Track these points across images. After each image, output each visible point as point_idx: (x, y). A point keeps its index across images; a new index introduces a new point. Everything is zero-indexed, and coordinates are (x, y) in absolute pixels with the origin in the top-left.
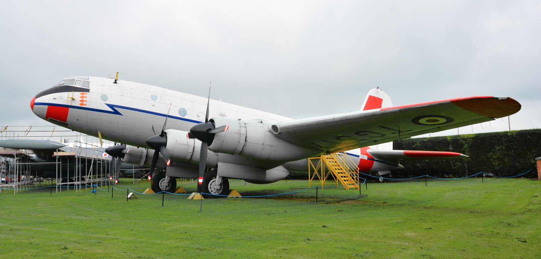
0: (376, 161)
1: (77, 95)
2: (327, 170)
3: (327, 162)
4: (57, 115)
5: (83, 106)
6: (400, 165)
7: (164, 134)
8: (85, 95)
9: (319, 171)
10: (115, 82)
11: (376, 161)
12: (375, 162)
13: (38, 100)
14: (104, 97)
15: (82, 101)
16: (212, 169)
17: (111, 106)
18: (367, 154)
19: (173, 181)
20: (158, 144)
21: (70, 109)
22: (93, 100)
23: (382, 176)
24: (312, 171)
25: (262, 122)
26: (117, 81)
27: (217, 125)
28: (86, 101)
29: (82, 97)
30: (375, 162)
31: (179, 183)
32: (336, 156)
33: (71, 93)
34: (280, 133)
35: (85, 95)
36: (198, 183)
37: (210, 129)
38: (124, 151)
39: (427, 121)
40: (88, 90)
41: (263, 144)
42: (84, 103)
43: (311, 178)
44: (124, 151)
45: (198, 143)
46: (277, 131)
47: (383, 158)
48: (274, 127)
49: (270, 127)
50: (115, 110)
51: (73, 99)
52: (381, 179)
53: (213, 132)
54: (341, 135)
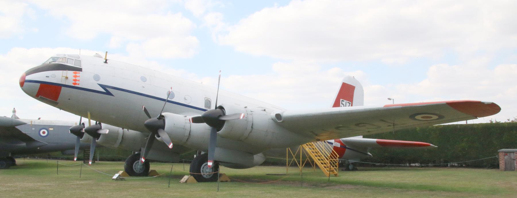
0: (348, 148)
1: (70, 74)
2: (304, 157)
3: (307, 149)
4: (48, 93)
5: (77, 86)
6: (369, 154)
7: (162, 117)
8: (78, 75)
9: (298, 157)
10: (106, 62)
11: (348, 148)
12: (347, 150)
13: (28, 78)
14: (97, 78)
15: (75, 80)
16: (203, 153)
17: (101, 86)
18: (340, 142)
19: (146, 165)
20: (156, 127)
21: (63, 88)
22: (86, 80)
23: (352, 164)
24: (290, 156)
25: (265, 110)
26: (108, 61)
27: (227, 113)
28: (79, 80)
29: (75, 76)
30: (347, 150)
31: (153, 167)
32: (315, 144)
33: (65, 72)
34: (283, 122)
35: (78, 75)
36: (209, 166)
37: (220, 116)
38: (101, 132)
39: (422, 117)
40: (80, 70)
41: (267, 131)
42: (77, 82)
43: (302, 165)
44: (101, 132)
45: (204, 127)
46: (281, 119)
47: (356, 147)
48: (278, 116)
49: (273, 115)
50: (107, 91)
51: (67, 78)
52: (351, 167)
53: (223, 118)
54: (341, 126)
